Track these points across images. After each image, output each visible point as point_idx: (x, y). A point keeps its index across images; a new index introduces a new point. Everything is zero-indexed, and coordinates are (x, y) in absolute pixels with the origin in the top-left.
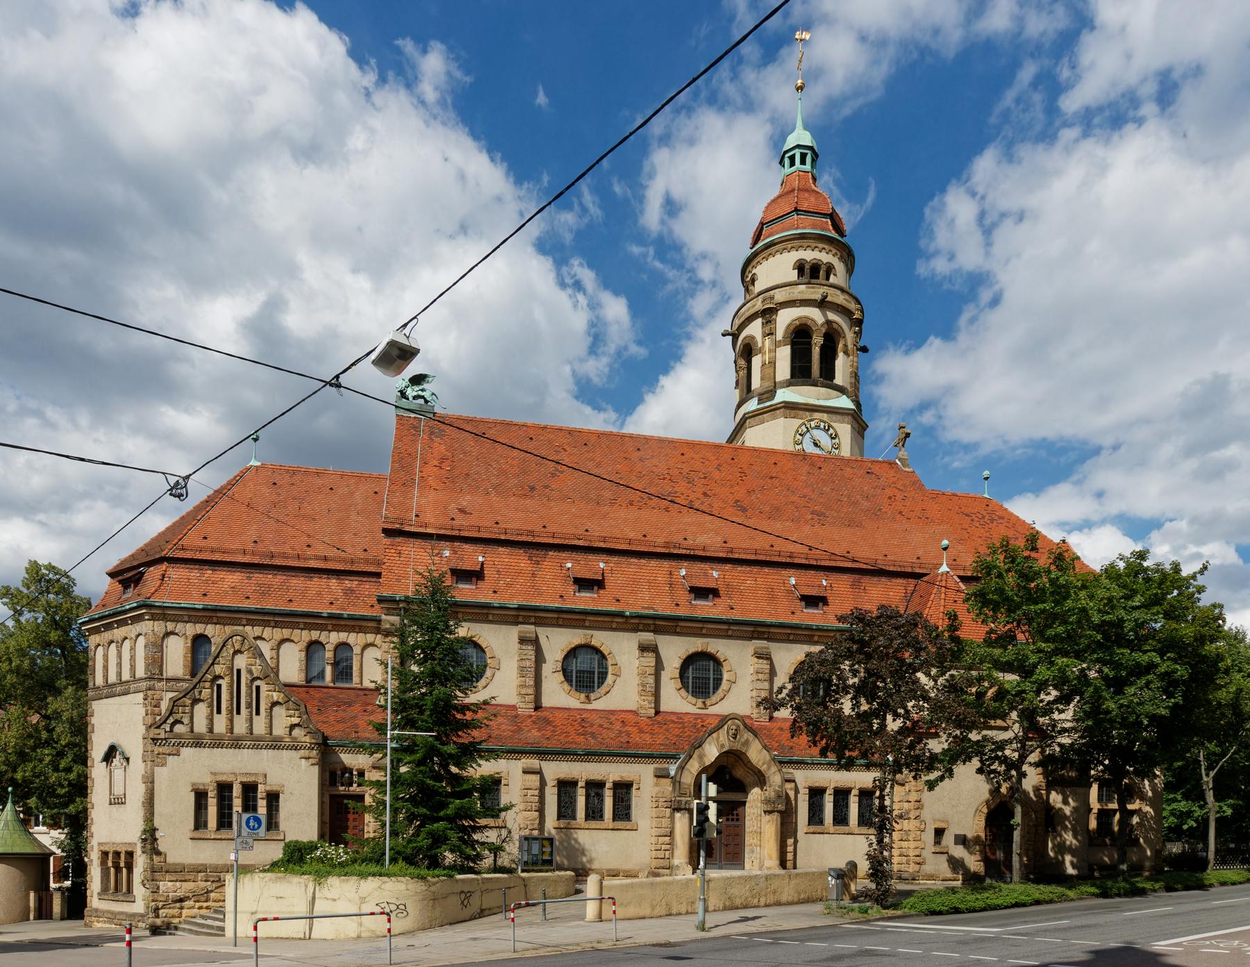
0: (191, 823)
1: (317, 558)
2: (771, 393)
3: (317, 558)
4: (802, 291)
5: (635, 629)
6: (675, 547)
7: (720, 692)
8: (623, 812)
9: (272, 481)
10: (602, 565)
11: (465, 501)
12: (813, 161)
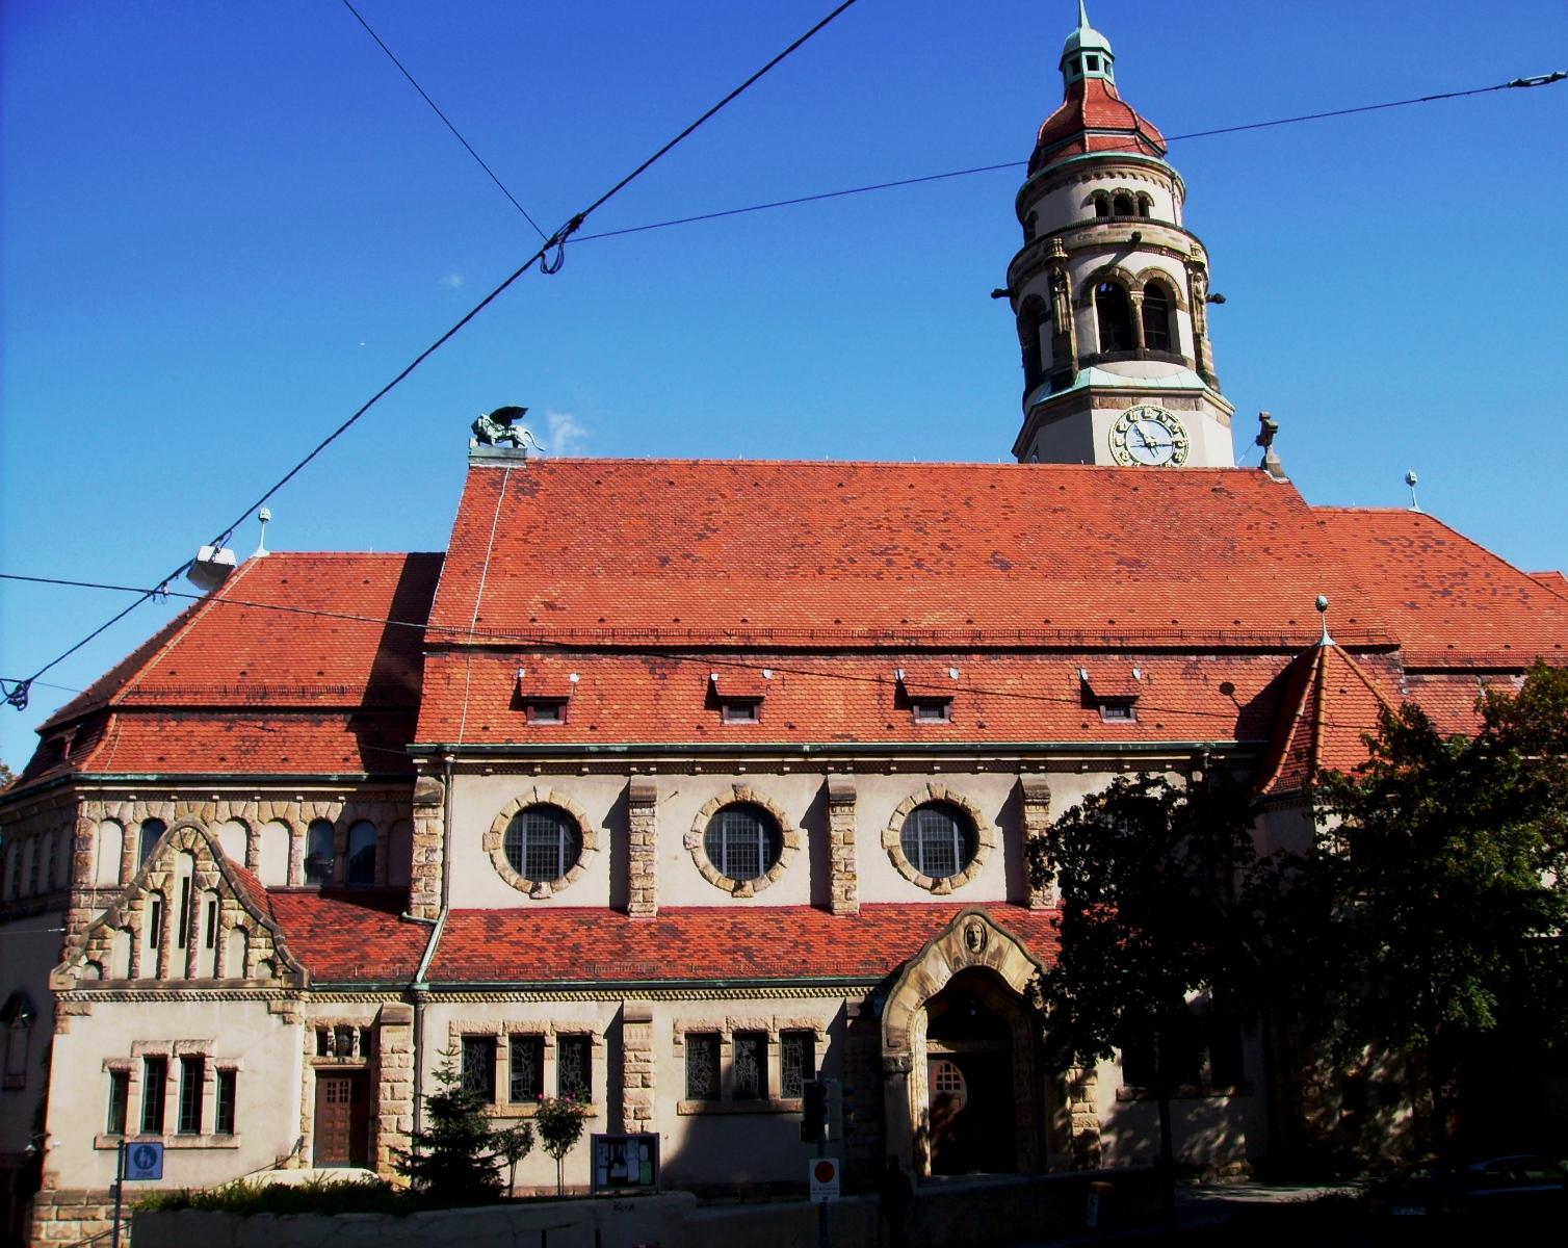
1: (330, 690)
3: (330, 690)
6: (886, 636)
9: (282, 578)
11: (554, 592)
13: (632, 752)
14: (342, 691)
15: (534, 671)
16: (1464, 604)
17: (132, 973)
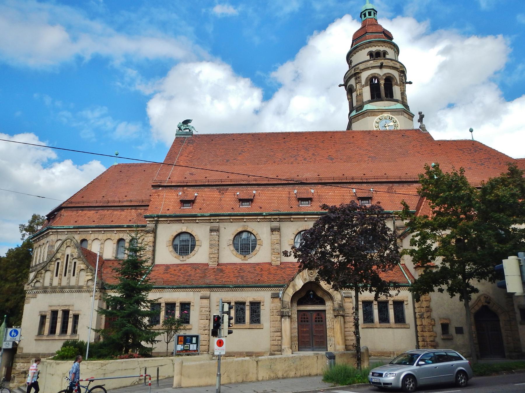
0: (36, 332)
2: (361, 107)
3: (127, 201)
4: (372, 63)
5: (270, 220)
7: (254, 252)
8: (256, 319)
10: (254, 192)
12: (374, 14)
13: (211, 216)
14: (131, 201)
15: (184, 193)
16: (489, 168)
17: (51, 284)
